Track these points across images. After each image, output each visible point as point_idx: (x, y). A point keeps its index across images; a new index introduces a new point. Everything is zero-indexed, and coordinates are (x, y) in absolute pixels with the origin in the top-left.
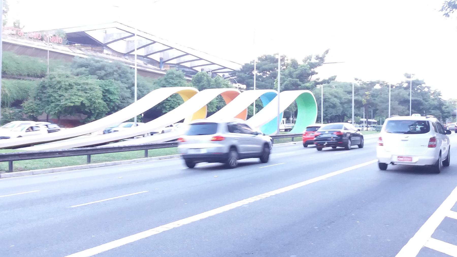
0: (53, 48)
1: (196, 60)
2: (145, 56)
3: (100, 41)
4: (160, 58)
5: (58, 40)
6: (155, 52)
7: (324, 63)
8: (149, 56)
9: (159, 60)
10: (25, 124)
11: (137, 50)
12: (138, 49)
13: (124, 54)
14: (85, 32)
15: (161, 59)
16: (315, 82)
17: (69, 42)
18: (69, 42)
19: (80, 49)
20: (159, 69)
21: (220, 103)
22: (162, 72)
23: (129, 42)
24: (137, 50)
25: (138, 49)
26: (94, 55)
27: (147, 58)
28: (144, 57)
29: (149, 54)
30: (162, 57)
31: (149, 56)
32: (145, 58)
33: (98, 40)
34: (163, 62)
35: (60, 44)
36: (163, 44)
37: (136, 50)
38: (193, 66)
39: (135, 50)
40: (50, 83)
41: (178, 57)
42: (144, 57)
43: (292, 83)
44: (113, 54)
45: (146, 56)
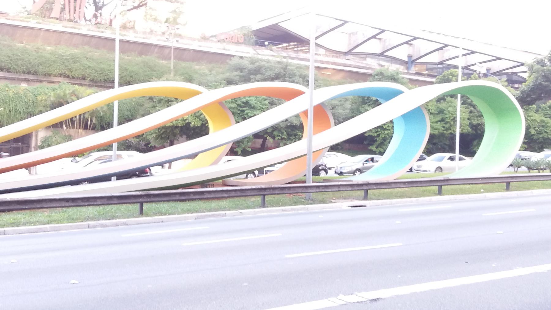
0: (224, 49)
1: (467, 53)
2: (380, 53)
3: (307, 38)
4: (408, 55)
5: (238, 38)
6: (393, 47)
7: (338, 297)
8: (386, 54)
9: (406, 59)
10: (222, 146)
11: (459, 56)
12: (458, 57)
13: (345, 52)
14: (278, 24)
15: (410, 57)
16: (64, 95)
17: (260, 40)
18: (260, 40)
19: (271, 49)
20: (406, 71)
21: (479, 118)
22: (409, 75)
23: (352, 35)
24: (459, 56)
25: (458, 57)
26: (292, 56)
27: (384, 57)
28: (379, 55)
29: (386, 50)
30: (411, 54)
31: (386, 54)
32: (380, 57)
33: (297, 33)
34: (412, 61)
35: (241, 43)
36: (395, 32)
37: (461, 56)
38: (468, 64)
39: (460, 57)
40: (4, 103)
41: (432, 51)
42: (379, 56)
43: (543, 74)
44: (327, 54)
45: (382, 54)
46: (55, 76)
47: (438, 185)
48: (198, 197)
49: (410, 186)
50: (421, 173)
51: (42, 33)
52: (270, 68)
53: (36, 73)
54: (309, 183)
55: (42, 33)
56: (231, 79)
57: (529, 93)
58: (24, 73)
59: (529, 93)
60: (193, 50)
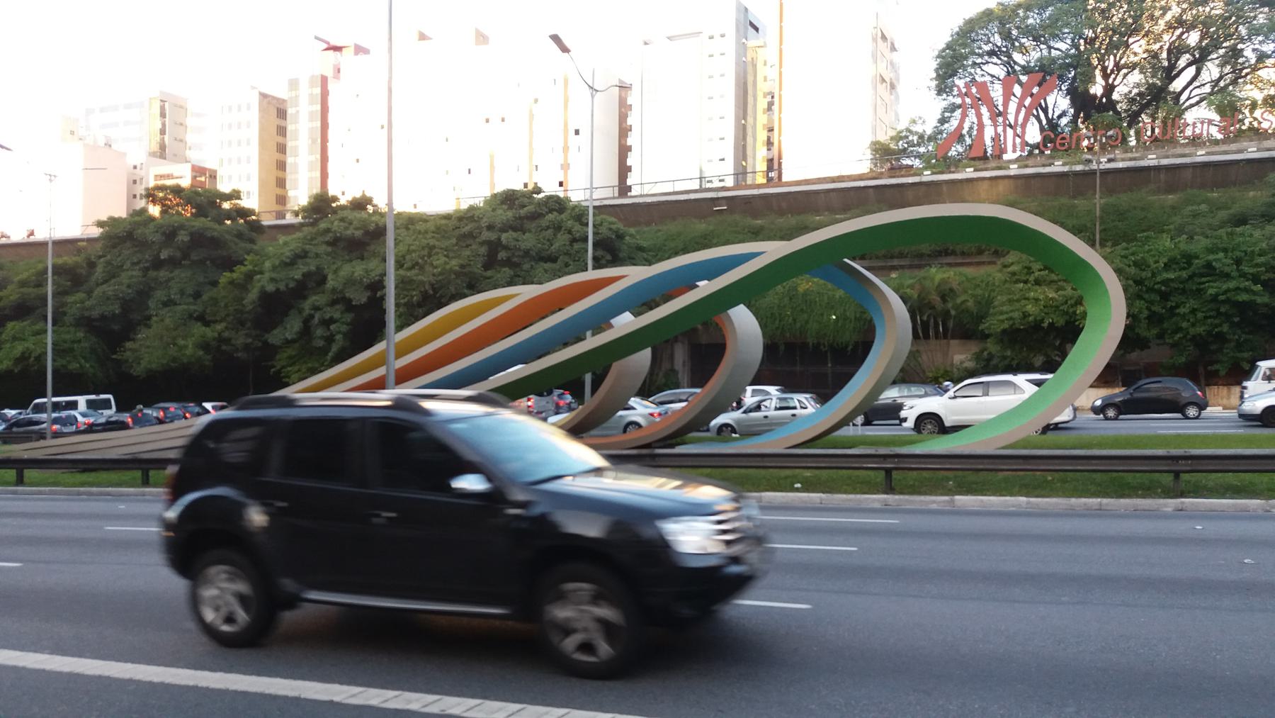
53: (901, 256)
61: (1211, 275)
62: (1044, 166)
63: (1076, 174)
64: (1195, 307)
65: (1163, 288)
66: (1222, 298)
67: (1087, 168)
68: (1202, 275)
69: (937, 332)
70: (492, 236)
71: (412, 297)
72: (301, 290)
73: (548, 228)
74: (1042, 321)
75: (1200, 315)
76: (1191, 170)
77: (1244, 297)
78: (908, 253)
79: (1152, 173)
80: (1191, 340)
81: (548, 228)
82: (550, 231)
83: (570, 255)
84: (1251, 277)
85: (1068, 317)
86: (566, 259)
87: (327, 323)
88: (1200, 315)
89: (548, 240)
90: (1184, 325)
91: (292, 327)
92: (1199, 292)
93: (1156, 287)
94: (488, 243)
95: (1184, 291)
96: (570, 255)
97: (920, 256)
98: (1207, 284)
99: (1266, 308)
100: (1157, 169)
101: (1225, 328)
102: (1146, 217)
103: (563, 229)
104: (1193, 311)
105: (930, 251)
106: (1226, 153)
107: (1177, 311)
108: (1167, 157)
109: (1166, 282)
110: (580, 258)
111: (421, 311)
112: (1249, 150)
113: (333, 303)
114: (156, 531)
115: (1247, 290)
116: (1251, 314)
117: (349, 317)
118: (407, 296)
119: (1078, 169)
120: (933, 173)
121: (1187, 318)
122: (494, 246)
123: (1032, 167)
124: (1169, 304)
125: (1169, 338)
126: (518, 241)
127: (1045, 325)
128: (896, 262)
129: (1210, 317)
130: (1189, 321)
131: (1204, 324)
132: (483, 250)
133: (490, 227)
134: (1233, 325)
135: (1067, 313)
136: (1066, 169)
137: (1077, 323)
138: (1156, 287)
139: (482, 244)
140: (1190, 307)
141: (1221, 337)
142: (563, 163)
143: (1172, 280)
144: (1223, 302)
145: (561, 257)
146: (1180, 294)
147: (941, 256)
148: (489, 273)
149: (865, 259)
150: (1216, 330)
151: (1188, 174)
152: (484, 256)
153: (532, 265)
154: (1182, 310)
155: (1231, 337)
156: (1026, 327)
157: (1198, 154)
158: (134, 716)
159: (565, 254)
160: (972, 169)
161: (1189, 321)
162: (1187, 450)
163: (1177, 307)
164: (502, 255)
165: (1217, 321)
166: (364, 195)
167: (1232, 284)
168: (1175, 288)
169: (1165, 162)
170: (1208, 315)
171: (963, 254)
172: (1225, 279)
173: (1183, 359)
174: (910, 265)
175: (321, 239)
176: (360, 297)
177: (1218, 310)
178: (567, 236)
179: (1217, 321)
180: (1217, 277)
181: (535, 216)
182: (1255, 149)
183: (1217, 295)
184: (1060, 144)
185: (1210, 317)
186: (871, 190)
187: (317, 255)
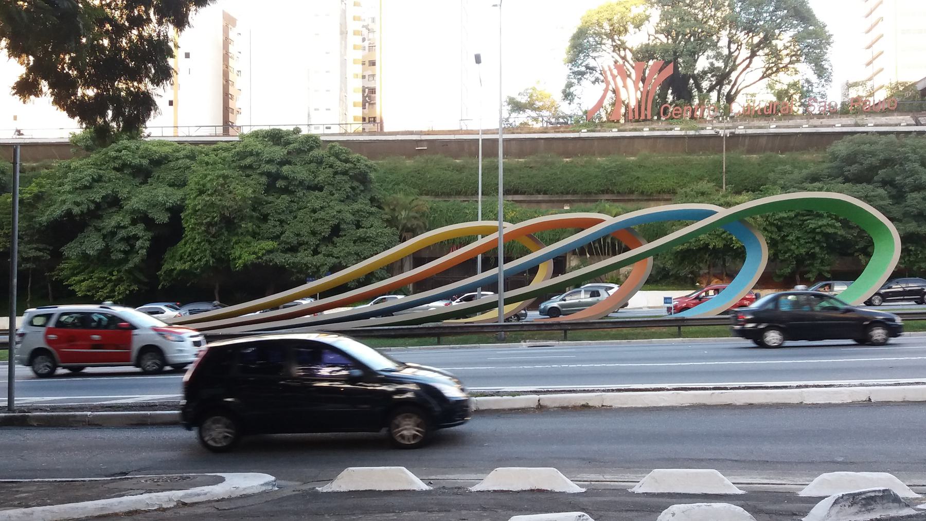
46: (596, 194)
47: (815, 311)
48: (366, 334)
49: (647, 326)
50: (596, 319)
51: (596, 143)
52: (873, 154)
53: (575, 192)
54: (500, 322)
55: (596, 143)
56: (817, 174)
57: (119, 303)
58: (562, 193)
59: (119, 303)
60: (801, 135)
61: (809, 215)
62: (666, 130)
63: (690, 137)
64: (799, 236)
65: (779, 223)
66: (818, 230)
67: (697, 134)
68: (803, 215)
69: (605, 253)
70: (273, 168)
71: (214, 218)
72: (96, 212)
73: (311, 162)
74: (708, 245)
75: (802, 241)
76: (766, 138)
77: (830, 230)
78: (579, 191)
79: (741, 138)
80: (795, 257)
81: (311, 162)
82: (313, 165)
83: (333, 185)
84: (834, 217)
85: (725, 242)
86: (331, 188)
87: (130, 240)
88: (802, 241)
89: (313, 172)
90: (793, 247)
91: (92, 244)
92: (801, 226)
93: (775, 222)
94: (268, 174)
95: (791, 226)
96: (333, 185)
97: (589, 193)
98: (808, 221)
99: (841, 238)
100: (744, 136)
101: (817, 250)
102: (742, 171)
103: (324, 164)
104: (798, 238)
105: (596, 190)
106: (788, 127)
107: (788, 238)
108: (750, 128)
109: (781, 219)
110: (341, 188)
111: (214, 229)
112: (804, 126)
113: (134, 222)
114: (178, 414)
115: (833, 226)
116: (832, 241)
117: (149, 235)
118: (209, 217)
119: (691, 134)
120: (588, 131)
121: (794, 243)
122: (273, 177)
123: (658, 130)
124: (783, 234)
125: (781, 256)
126: (294, 173)
127: (711, 247)
128: (569, 197)
129: (809, 242)
130: (795, 245)
131: (804, 247)
132: (264, 180)
133: (270, 161)
134: (822, 248)
135: (724, 239)
136: (683, 133)
137: (732, 246)
138: (775, 222)
139: (262, 174)
140: (795, 236)
141: (813, 256)
142: (179, 91)
143: (784, 218)
144: (818, 233)
145: (326, 187)
146: (789, 227)
147: (603, 194)
148: (270, 198)
149: (547, 194)
150: (812, 251)
151: (763, 141)
152: (264, 185)
153: (304, 193)
154: (790, 238)
155: (820, 255)
156: (697, 248)
157: (771, 127)
158: (453, 520)
159: (329, 184)
160: (617, 130)
161: (919, 254)
162: (642, 331)
163: (787, 236)
164: (280, 184)
165: (812, 246)
166: (73, 118)
167: (824, 222)
168: (787, 223)
169: (750, 131)
170: (807, 241)
171: (618, 193)
172: (818, 218)
173: (789, 271)
174: (580, 200)
175: (112, 165)
176: (162, 218)
177: (814, 238)
178: (330, 171)
179: (812, 246)
180: (812, 217)
181: (299, 151)
182: (807, 126)
183: (815, 229)
184: (675, 114)
185: (809, 242)
186: (542, 141)
187: (110, 180)
